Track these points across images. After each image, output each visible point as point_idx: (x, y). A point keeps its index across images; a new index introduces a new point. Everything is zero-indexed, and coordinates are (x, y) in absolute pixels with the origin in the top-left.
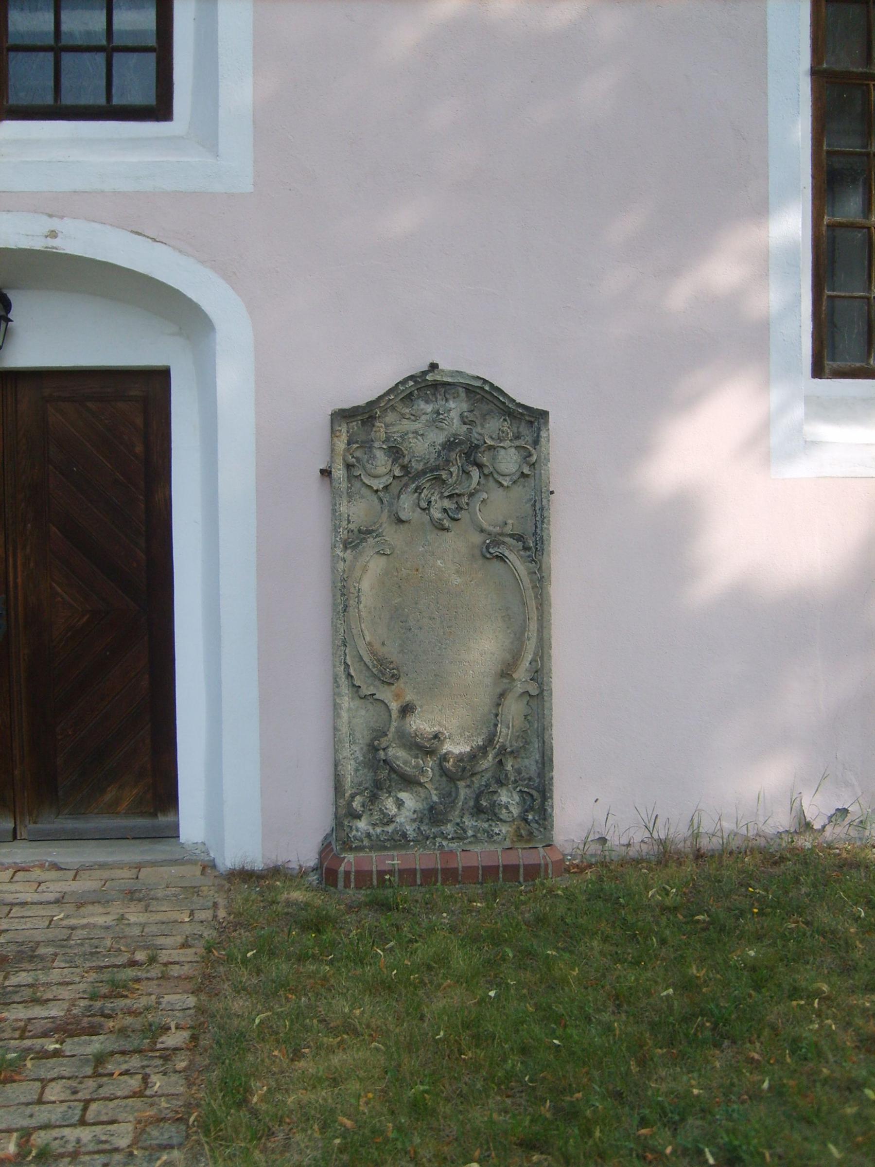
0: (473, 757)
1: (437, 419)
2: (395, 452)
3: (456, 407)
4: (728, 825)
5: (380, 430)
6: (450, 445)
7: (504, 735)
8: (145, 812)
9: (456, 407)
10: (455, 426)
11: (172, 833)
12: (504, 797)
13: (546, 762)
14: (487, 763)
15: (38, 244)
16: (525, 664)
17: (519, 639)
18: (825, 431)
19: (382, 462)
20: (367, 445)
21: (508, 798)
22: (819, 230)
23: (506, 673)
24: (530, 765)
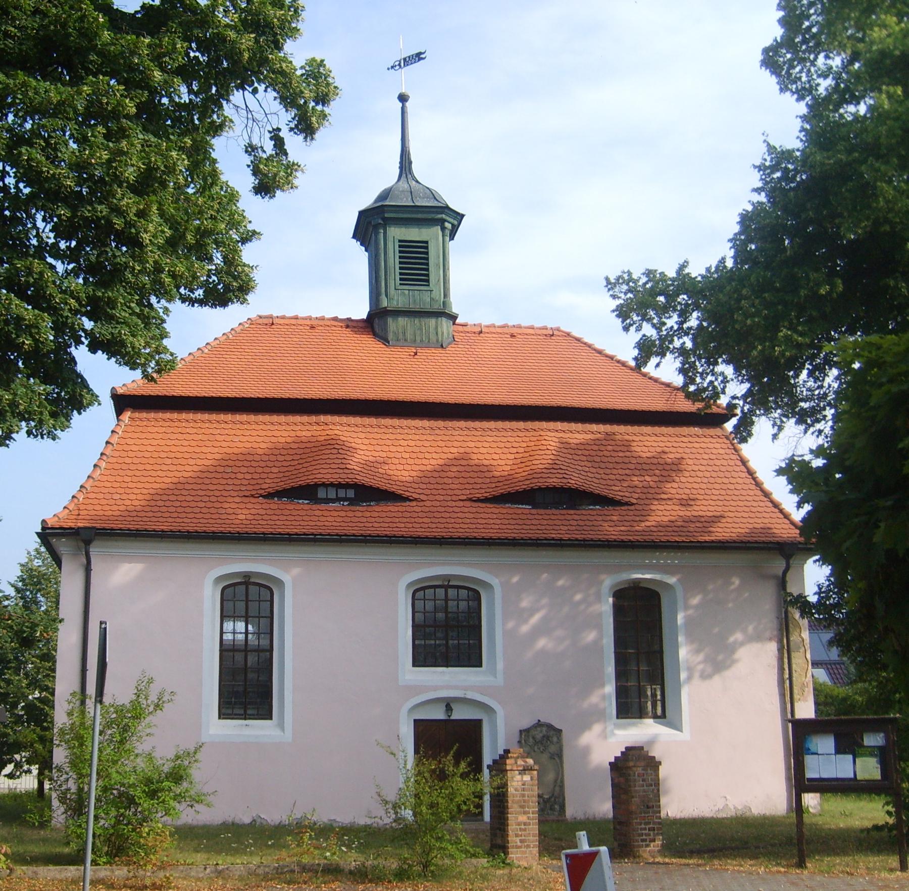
0: (550, 798)
1: (541, 731)
2: (534, 738)
3: (544, 729)
4: (601, 816)
5: (530, 734)
6: (544, 736)
7: (556, 794)
8: (558, 738)
9: (544, 729)
10: (544, 732)
11: (483, 820)
12: (556, 806)
13: (564, 799)
14: (553, 799)
15: (463, 696)
16: (559, 780)
17: (558, 774)
18: (617, 732)
19: (531, 740)
20: (528, 737)
21: (556, 807)
22: (351, 872)
23: (556, 781)
24: (561, 800)
